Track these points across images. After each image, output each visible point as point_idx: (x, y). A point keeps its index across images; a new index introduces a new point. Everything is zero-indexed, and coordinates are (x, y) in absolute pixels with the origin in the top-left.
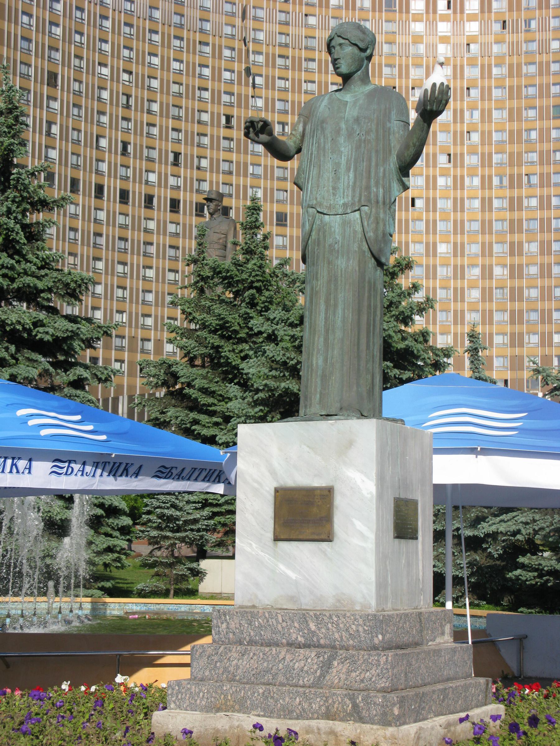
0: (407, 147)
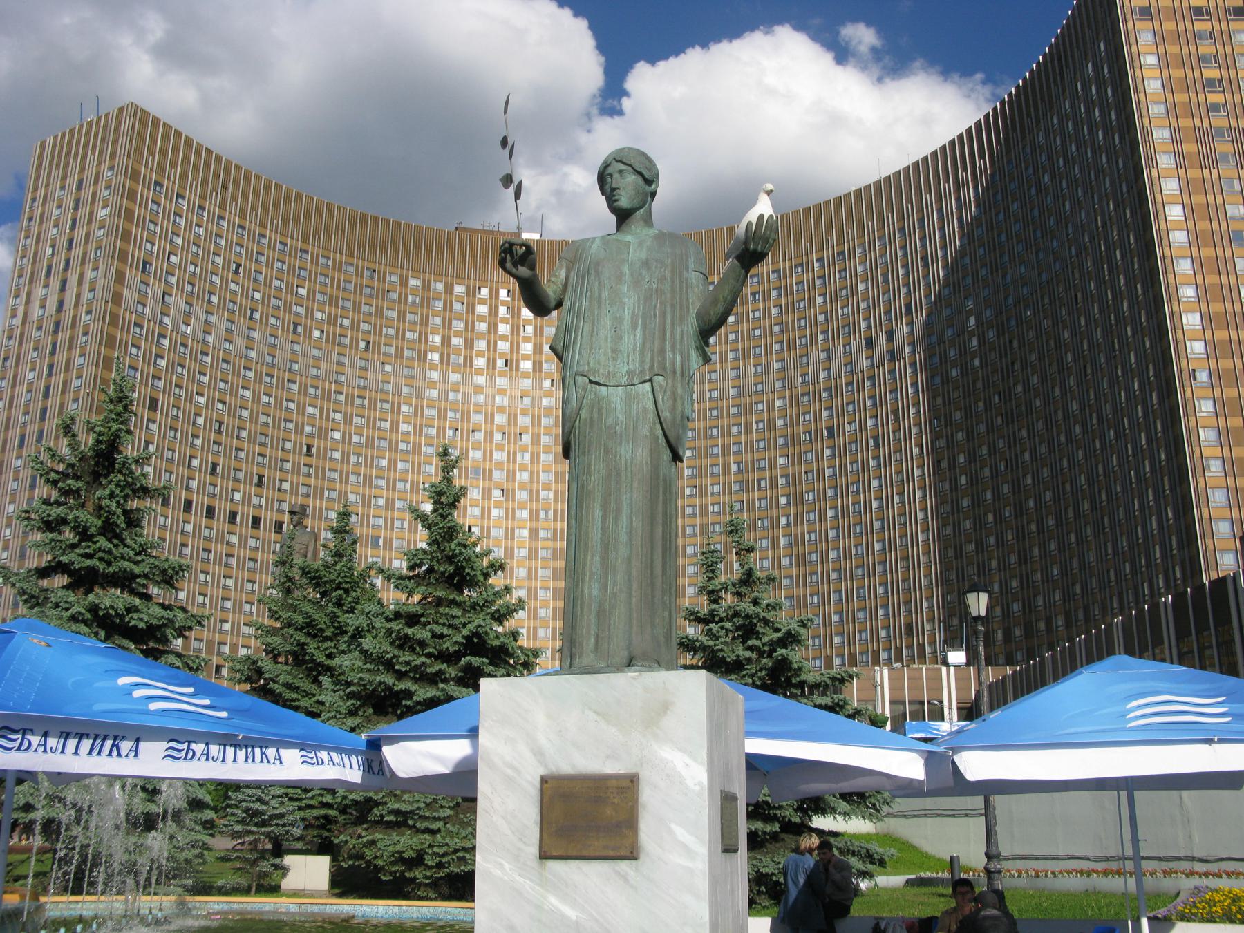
0: (715, 302)
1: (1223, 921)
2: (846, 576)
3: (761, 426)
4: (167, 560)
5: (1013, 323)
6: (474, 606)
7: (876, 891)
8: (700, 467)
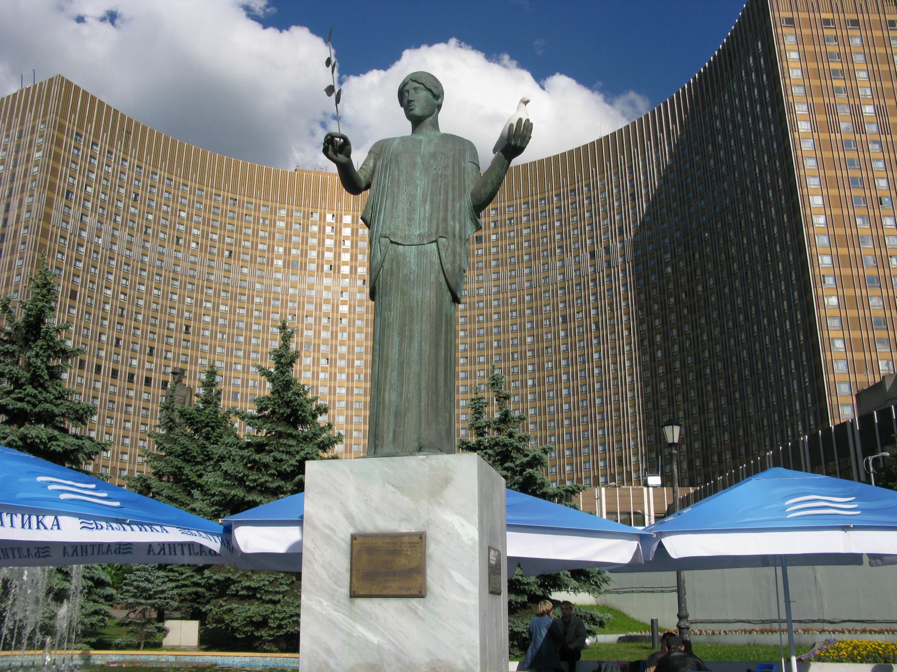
0: (485, 184)
1: (848, 661)
2: (574, 422)
3: (514, 314)
4: (79, 403)
5: (696, 241)
6: (305, 438)
7: (597, 646)
8: (471, 344)
